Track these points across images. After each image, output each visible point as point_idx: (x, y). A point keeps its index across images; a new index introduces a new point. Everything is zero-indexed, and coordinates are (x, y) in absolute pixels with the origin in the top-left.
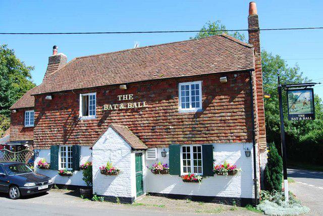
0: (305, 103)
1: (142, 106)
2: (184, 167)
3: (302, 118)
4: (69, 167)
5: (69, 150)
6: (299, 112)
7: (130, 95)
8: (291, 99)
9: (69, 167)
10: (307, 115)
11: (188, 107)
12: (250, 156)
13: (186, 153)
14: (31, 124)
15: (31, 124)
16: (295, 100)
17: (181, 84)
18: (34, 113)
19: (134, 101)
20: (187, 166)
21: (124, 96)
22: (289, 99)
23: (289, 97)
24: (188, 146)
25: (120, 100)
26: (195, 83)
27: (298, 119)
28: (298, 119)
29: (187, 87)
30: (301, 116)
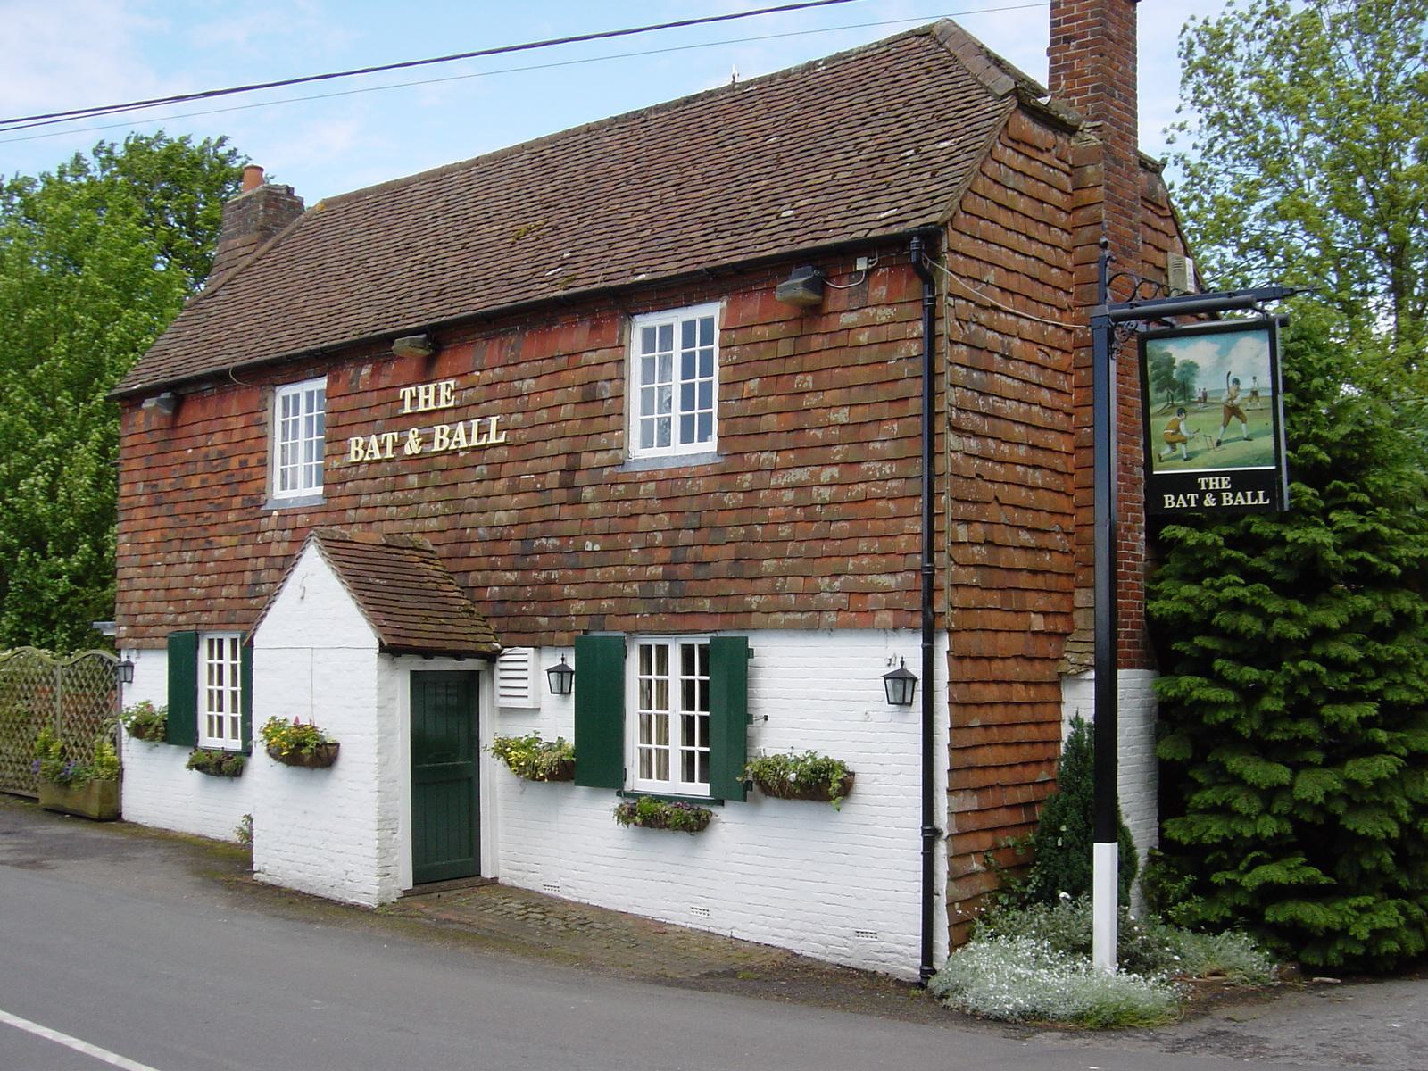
0: (1233, 411)
1: (483, 442)
2: (667, 743)
3: (1217, 494)
4: (689, 777)
5: (688, 668)
6: (1200, 459)
7: (443, 385)
8: (1159, 390)
9: (689, 777)
10: (1241, 481)
11: (665, 441)
12: (911, 704)
13: (654, 677)
14: (687, 437)
15: (687, 437)
16: (1181, 387)
17: (642, 322)
18: (1300, 234)
19: (460, 412)
20: (654, 746)
21: (422, 388)
22: (1152, 388)
23: (1150, 373)
24: (662, 642)
25: (407, 410)
26: (697, 313)
27: (1200, 501)
28: (1200, 501)
29: (667, 331)
30: (1214, 483)
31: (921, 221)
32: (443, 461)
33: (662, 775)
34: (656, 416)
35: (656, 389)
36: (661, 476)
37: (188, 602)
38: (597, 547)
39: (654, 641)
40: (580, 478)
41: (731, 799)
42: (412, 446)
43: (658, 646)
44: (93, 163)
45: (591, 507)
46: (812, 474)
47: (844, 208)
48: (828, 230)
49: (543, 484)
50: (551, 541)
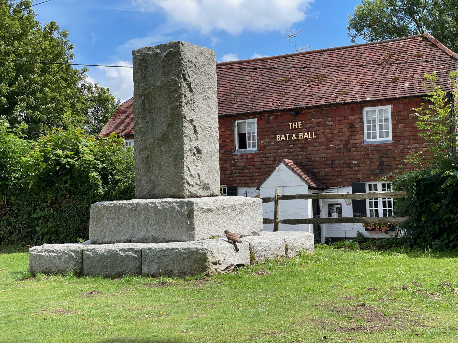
12: (341, 204)
31: (360, 100)
32: (303, 142)
33: (372, 211)
34: (384, 131)
35: (371, 126)
36: (374, 146)
37: (363, 160)
38: (356, 162)
39: (373, 183)
40: (349, 146)
41: (314, 226)
42: (294, 137)
43: (374, 184)
44: (308, 6)
45: (354, 153)
46: (420, 145)
47: (273, 100)
48: (422, 91)
49: (338, 147)
50: (341, 161)
